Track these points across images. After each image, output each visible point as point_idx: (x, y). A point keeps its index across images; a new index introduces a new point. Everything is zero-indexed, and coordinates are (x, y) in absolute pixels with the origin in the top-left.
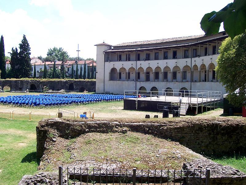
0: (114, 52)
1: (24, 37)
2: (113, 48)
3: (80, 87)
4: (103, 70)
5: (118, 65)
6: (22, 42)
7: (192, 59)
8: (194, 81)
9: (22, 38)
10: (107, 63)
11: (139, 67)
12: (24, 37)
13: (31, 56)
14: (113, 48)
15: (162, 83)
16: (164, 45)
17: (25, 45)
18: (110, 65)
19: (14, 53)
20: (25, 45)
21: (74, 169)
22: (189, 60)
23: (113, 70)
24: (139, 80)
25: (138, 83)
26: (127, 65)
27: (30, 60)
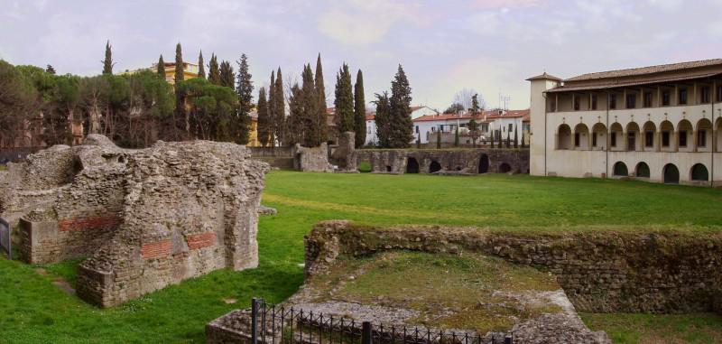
0: (586, 90)
1: (400, 69)
2: (562, 84)
3: (501, 162)
4: (545, 127)
5: (572, 118)
6: (397, 78)
7: (715, 105)
8: (132, 145)
9: (397, 71)
10: (551, 115)
11: (612, 121)
12: (400, 69)
13: (412, 104)
14: (562, 84)
15: (657, 154)
16: (621, 82)
17: (401, 84)
18: (557, 119)
19: (382, 102)
20: (401, 84)
21: (292, 310)
22: (708, 107)
23: (564, 129)
24: (613, 149)
25: (611, 155)
26: (590, 118)
27: (410, 110)
